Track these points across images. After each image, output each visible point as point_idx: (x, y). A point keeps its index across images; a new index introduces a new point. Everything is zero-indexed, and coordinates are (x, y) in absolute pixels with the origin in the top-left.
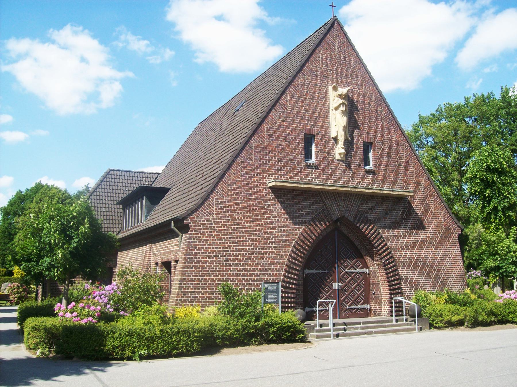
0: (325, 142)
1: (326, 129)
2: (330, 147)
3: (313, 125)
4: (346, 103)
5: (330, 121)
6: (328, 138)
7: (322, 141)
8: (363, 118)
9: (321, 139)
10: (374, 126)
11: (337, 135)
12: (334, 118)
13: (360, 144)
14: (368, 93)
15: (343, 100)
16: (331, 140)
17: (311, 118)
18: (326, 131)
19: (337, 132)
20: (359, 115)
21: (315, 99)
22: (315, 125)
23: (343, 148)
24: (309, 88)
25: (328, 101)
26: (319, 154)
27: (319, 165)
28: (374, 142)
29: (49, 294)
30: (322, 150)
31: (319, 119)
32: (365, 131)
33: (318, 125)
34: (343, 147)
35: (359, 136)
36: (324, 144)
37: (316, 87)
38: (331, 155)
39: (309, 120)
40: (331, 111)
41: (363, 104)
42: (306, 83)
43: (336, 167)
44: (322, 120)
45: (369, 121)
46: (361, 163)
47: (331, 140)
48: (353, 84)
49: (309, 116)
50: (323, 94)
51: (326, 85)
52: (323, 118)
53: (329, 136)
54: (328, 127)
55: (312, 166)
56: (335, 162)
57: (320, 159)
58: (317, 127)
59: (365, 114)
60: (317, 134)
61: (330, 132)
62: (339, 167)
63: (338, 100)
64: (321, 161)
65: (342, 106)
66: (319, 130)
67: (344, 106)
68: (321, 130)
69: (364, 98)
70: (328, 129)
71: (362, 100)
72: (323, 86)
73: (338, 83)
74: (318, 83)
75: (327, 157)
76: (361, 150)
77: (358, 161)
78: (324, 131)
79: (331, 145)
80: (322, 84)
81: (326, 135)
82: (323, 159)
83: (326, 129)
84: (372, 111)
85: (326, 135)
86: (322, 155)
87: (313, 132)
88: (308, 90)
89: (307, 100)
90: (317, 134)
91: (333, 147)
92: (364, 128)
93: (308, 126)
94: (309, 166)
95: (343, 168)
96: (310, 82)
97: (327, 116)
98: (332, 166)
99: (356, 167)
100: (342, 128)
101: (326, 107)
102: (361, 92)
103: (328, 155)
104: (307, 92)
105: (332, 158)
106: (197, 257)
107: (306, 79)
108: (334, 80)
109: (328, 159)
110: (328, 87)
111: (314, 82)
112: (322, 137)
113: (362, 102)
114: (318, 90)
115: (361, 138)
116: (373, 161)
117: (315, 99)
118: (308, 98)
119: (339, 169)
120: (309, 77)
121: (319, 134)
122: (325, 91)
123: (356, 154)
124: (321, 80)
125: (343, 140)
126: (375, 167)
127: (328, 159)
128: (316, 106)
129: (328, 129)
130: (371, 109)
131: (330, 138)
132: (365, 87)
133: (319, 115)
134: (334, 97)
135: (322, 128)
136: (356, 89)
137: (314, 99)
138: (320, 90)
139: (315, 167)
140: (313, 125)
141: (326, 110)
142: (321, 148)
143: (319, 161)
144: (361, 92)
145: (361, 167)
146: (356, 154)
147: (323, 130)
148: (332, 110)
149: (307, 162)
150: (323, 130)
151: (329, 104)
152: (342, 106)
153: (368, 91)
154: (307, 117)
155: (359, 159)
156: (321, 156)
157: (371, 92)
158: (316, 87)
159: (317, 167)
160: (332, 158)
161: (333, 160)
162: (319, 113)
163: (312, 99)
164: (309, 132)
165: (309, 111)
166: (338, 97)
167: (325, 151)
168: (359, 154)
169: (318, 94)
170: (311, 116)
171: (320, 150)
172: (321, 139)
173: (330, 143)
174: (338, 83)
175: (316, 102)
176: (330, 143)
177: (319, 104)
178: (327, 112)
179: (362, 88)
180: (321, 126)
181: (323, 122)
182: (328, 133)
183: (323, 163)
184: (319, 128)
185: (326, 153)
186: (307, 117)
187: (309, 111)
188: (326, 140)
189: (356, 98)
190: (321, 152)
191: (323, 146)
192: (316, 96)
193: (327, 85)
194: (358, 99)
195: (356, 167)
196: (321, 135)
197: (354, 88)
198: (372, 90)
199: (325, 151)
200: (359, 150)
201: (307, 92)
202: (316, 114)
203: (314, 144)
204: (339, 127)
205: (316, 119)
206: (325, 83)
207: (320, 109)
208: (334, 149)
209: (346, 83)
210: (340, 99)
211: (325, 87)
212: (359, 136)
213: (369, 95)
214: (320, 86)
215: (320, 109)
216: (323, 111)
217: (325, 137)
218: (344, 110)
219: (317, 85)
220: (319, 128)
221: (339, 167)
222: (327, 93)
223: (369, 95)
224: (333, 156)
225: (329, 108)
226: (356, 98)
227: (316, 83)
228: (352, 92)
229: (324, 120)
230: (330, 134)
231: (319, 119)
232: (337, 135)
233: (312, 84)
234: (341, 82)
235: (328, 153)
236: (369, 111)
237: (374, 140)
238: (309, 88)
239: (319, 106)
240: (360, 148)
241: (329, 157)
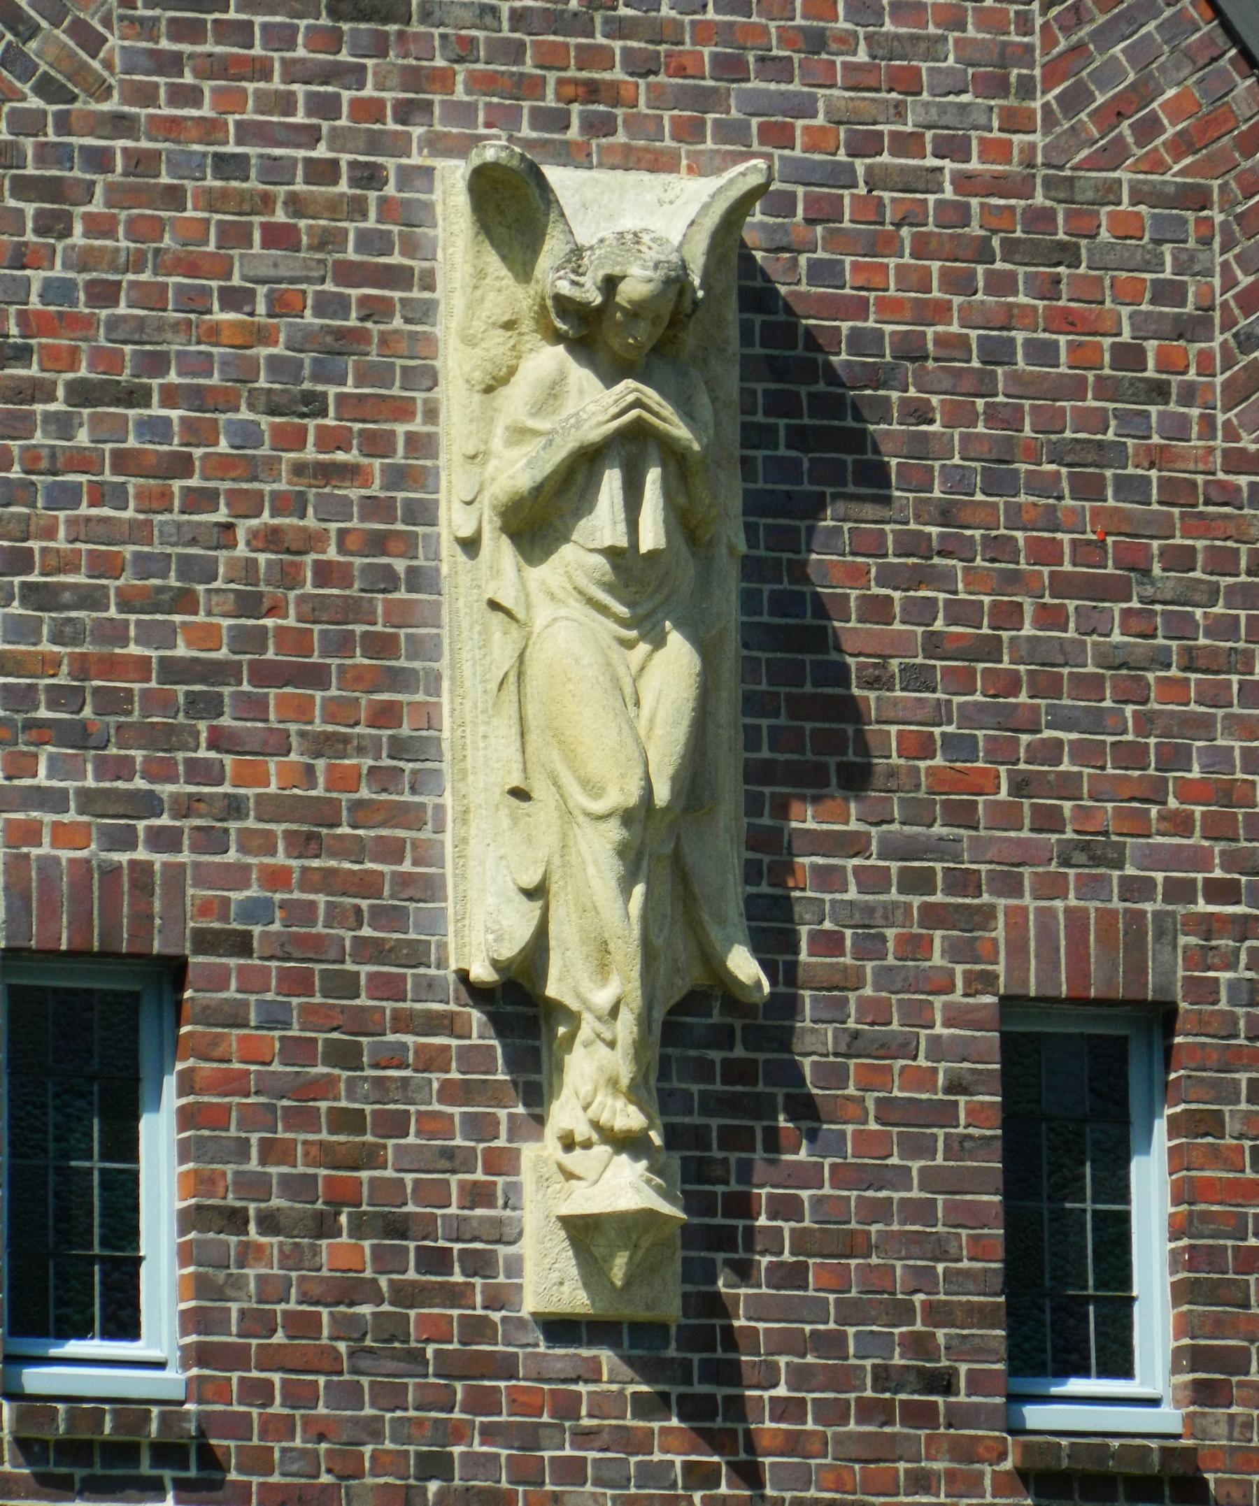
0: (346, 1056)
1: (357, 850)
2: (435, 1125)
3: (148, 804)
4: (680, 430)
5: (430, 718)
6: (390, 988)
7: (297, 1050)
8: (1009, 615)
9: (274, 1018)
10: (1203, 726)
11: (539, 944)
12: (503, 657)
13: (938, 1049)
14: (1110, 192)
15: (628, 388)
16: (447, 1024)
17: (111, 702)
18: (368, 885)
19: (537, 893)
20: (943, 580)
21: (198, 398)
22: (185, 807)
23: (628, 1143)
24: (100, 227)
25: (403, 410)
26: (247, 1254)
27: (240, 1425)
28: (1205, 991)
29: (700, 294)
30: (299, 1187)
31: (256, 707)
32: (1048, 820)
33: (235, 807)
34: (630, 1118)
35: (933, 917)
36: (324, 1087)
37: (212, 201)
38: (436, 1260)
39: (78, 736)
40: (450, 559)
41: (1023, 386)
42: (45, 154)
43: (530, 1438)
44: (302, 711)
45: (1113, 660)
46: (957, 1349)
47: (447, 1024)
48: (858, 80)
49: (82, 667)
50: (325, 305)
51: (376, 143)
52: (318, 677)
53: (416, 955)
54: (410, 816)
55: (124, 1452)
56: (506, 1367)
57: (259, 1323)
58: (212, 841)
59: (1046, 553)
60: (206, 942)
61: (430, 888)
62: (584, 1437)
63: (553, 392)
64: (270, 1359)
65: (612, 482)
66: (239, 876)
67: (653, 476)
68: (276, 878)
69: (1051, 288)
70: (393, 851)
71: (1009, 318)
72: (324, 172)
73: (592, 91)
74: (246, 132)
75: (372, 1293)
76: (958, 1147)
77: (904, 1312)
78: (327, 881)
79: (450, 1092)
80: (311, 136)
81: (369, 950)
82: (303, 1325)
83: (357, 850)
84: (1176, 492)
85: (369, 950)
86: (291, 1259)
87: (143, 919)
88: (84, 261)
89: (63, 425)
90: (206, 942)
91: (481, 1127)
92: (1020, 786)
93: (63, 836)
94: (75, 1450)
95: (642, 1443)
96: (121, 124)
97: (382, 645)
98: (459, 1433)
99: (867, 1410)
100: (614, 832)
101: (373, 508)
102: (998, 186)
103: (386, 1260)
104: (53, 290)
105: (457, 1296)
106: (37, 277)
107: (47, 88)
108: (515, 52)
109: (393, 1329)
110: (408, 176)
111: (170, 128)
112: (298, 983)
113: (997, 353)
114: (235, 236)
115: (956, 952)
116: (1181, 1292)
117: (198, 398)
118: (82, 394)
119: (572, 1471)
120: (93, 43)
121: (242, 946)
122: (367, 241)
123: (881, 1210)
124: (293, 72)
125: (626, 1027)
126: (1205, 1394)
127: (393, 1329)
128: (200, 500)
129: (393, 851)
130: (1156, 458)
131: (430, 987)
132: (1073, 101)
133: (251, 640)
134: (497, 345)
135: (304, 844)
136: (907, 144)
137: (170, 397)
138: (279, 237)
139: (167, 1453)
140: (148, 804)
141: (379, 543)
142: (270, 1151)
143: (233, 1357)
144: (998, 186)
145: (957, 1417)
146: (881, 1210)
147: (309, 880)
148: (470, 545)
149: (36, 1379)
150: (309, 880)
151: (422, 445)
152: (612, 482)
153: (1114, 155)
154: (57, 697)
155: (922, 1281)
156: (271, 1290)
157: (1175, 173)
158: (212, 201)
159: (211, 1460)
160: (457, 1296)
161: (477, 1329)
162: (248, 604)
163: (137, 396)
164: (81, 921)
165: (91, 599)
166: (557, 337)
167: (342, 1196)
168: (922, 1211)
169: (233, 298)
170: (111, 666)
171: (256, 1186)
172: (274, 1018)
173: (432, 1060)
174: (592, 91)
175: (199, 433)
176: (432, 1060)
177: (252, 468)
178: (388, 580)
179: (1016, 122)
180: (272, 808)
181: (322, 745)
182: (392, 917)
183: (299, 1396)
184: (248, 842)
185: (359, 1228)
186: (57, 697)
187: (91, 599)
188: (363, 1023)
189: (889, 308)
190: (269, 1223)
191: (306, 1120)
192: (214, 334)
193: (400, 146)
194: (941, 311)
195: (867, 1410)
196: (282, 949)
197: (866, 145)
198: (1182, 145)
199: (342, 1196)
200: (923, 1148)
201: (56, 291)
202: (206, 637)
203: (171, 1098)
204: (567, 812)
205: (208, 706)
206: (365, 110)
207: (270, 539)
208: (502, 1162)
209: (731, 68)
210: (581, 376)
211: (369, 177)
212: (933, 917)
213: (1127, 229)
214: (276, 171)
215: (270, 539)
216: (324, 573)
217: (346, 985)
218: (651, 536)
219: (228, 166)
220: (248, 842)
221: (584, 1437)
222: (399, 277)
223: (1127, 229)
224: (479, 1264)
225: (424, 513)
226: (889, 308)
227: (210, 130)
228: (824, 213)
229: (334, 711)
230: (435, 922)
231: (256, 707)
232: (539, 944)
233: (141, 163)
234: (643, 67)
235: (398, 1227)
236: (1132, 488)
237: (1200, 958)
238: (100, 227)
239: (248, 505)
240: (945, 1114)
241: (406, 1295)
